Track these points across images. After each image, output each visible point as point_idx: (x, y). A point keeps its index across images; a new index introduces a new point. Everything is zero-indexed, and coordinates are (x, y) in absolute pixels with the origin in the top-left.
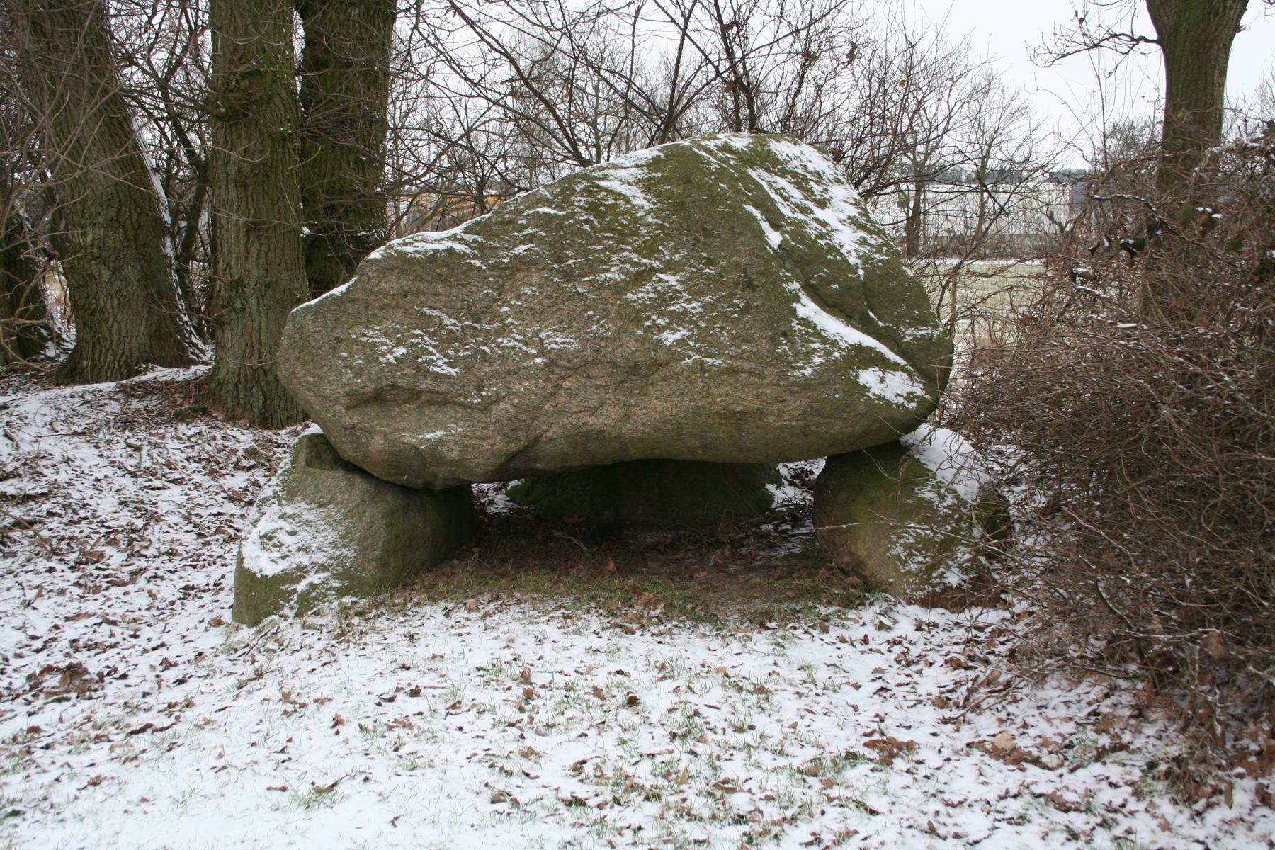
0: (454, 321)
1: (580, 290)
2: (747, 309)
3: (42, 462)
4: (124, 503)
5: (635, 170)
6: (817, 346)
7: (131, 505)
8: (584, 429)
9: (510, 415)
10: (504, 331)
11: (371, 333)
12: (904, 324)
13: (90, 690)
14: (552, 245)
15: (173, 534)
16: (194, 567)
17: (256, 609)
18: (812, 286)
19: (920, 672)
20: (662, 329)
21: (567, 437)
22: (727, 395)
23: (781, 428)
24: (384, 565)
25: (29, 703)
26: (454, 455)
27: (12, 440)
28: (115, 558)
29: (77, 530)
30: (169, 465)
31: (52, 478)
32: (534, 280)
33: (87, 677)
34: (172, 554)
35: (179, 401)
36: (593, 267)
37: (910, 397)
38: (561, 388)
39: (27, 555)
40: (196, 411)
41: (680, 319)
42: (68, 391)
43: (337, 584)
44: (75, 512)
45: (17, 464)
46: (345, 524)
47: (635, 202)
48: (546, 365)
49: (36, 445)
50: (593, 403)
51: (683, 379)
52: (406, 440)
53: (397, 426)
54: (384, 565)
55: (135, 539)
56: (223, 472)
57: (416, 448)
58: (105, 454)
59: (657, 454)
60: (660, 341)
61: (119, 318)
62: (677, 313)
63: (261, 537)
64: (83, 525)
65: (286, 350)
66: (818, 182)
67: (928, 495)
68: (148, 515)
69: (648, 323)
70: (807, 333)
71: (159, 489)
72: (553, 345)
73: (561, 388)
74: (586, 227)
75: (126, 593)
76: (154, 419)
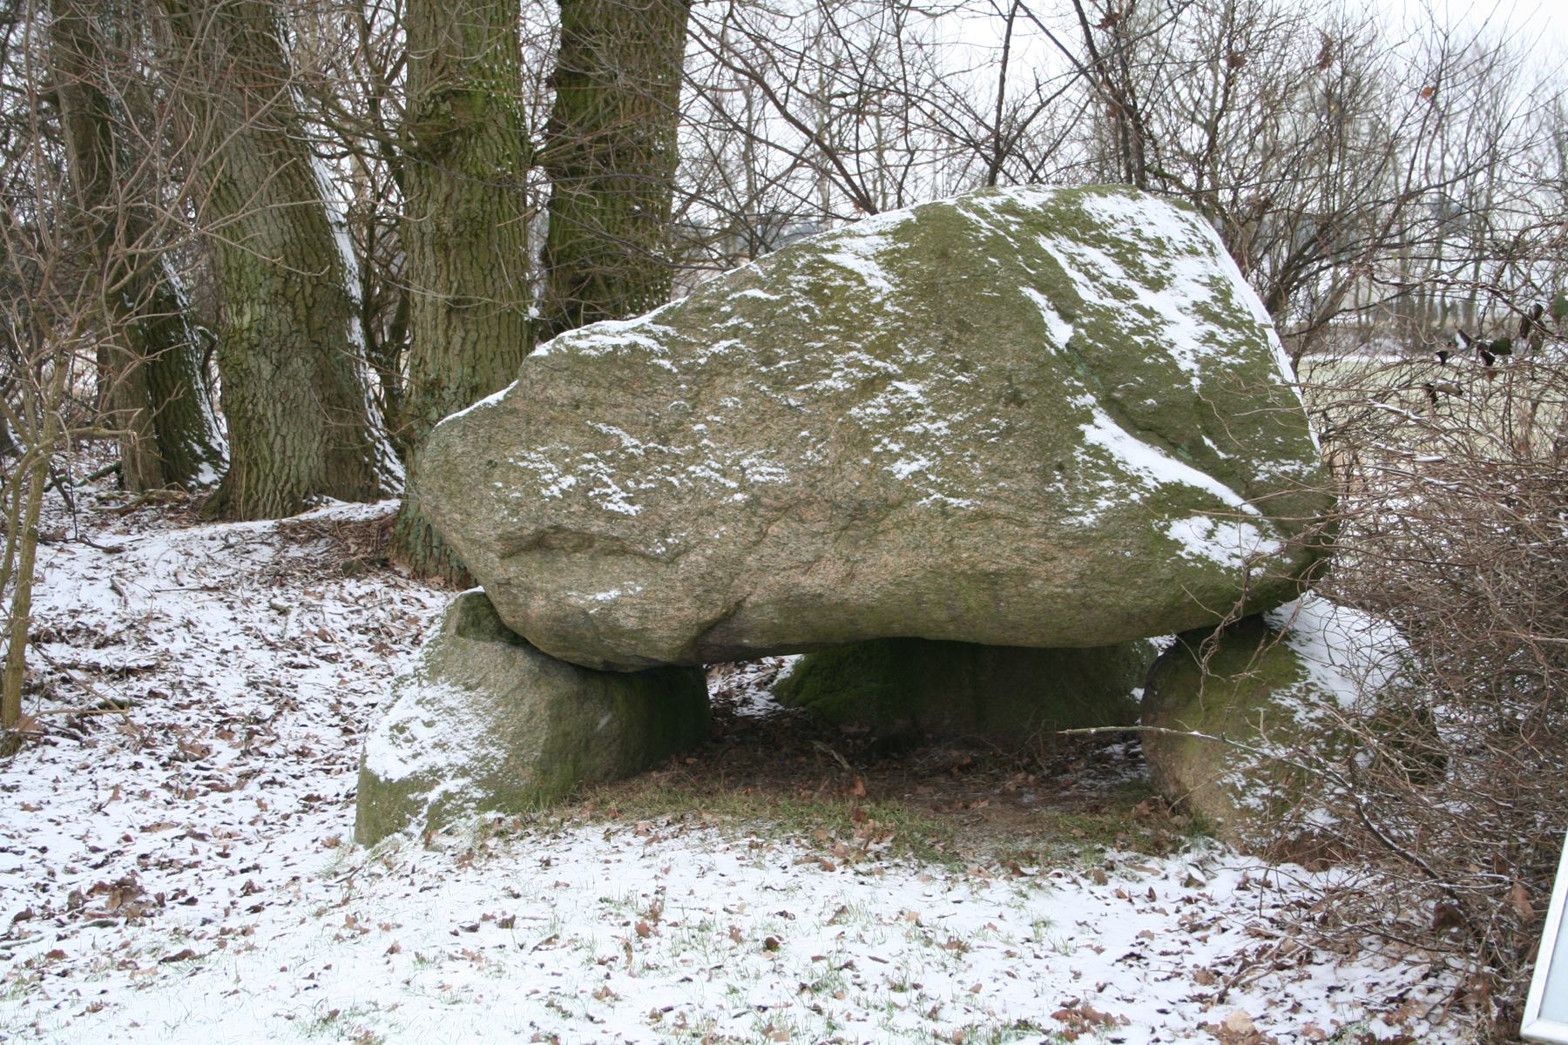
0: (636, 442)
1: (792, 402)
2: (1008, 432)
3: (153, 625)
4: (253, 685)
5: (878, 239)
6: (1106, 484)
7: (263, 688)
8: (795, 592)
9: (703, 570)
10: (697, 456)
11: (533, 455)
12: (1258, 457)
13: (143, 915)
14: (761, 340)
15: (312, 729)
16: (328, 772)
17: (377, 825)
18: (1115, 400)
19: (1204, 940)
20: (895, 457)
21: (775, 603)
22: (976, 549)
23: (1052, 596)
24: (544, 770)
25: (62, 924)
26: (631, 623)
27: (120, 594)
28: (225, 754)
29: (183, 717)
30: (323, 636)
31: (162, 646)
32: (737, 388)
33: (142, 898)
34: (302, 754)
35: (353, 548)
36: (810, 370)
37: (1255, 559)
38: (765, 535)
39: (110, 746)
40: (372, 563)
41: (920, 443)
42: (209, 530)
43: (479, 794)
44: (186, 693)
45: (121, 627)
46: (496, 713)
47: (870, 283)
48: (748, 504)
49: (149, 601)
50: (810, 557)
51: (919, 527)
52: (572, 601)
53: (563, 582)
54: (544, 772)
55: (257, 732)
56: (396, 647)
57: (585, 613)
58: (240, 617)
59: (897, 629)
60: (891, 473)
61: (284, 431)
62: (918, 439)
63: (391, 729)
64: (193, 712)
65: (428, 476)
66: (1153, 254)
67: (1288, 702)
68: (282, 701)
69: (877, 449)
70: (1096, 466)
71: (304, 667)
72: (757, 477)
73: (765, 535)
74: (804, 317)
75: (227, 801)
76: (315, 572)
